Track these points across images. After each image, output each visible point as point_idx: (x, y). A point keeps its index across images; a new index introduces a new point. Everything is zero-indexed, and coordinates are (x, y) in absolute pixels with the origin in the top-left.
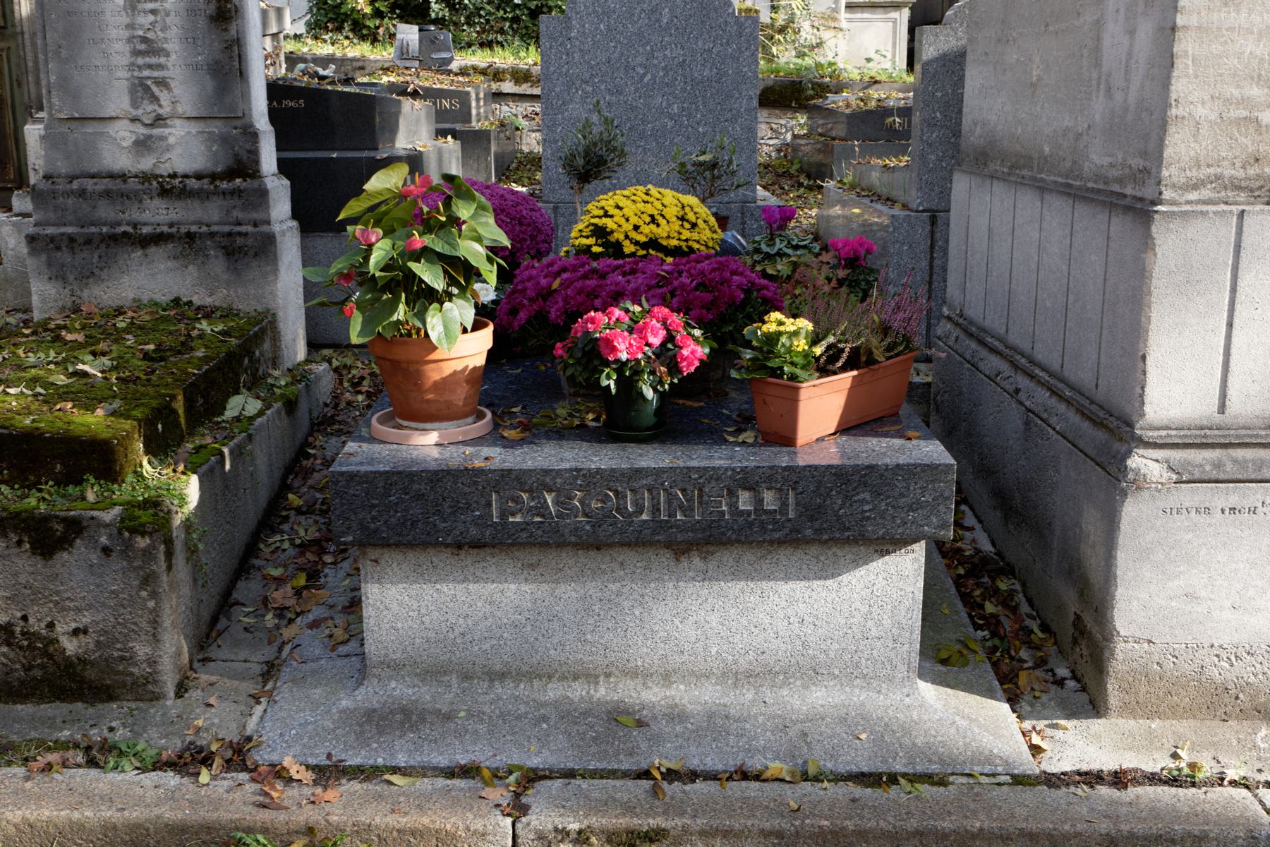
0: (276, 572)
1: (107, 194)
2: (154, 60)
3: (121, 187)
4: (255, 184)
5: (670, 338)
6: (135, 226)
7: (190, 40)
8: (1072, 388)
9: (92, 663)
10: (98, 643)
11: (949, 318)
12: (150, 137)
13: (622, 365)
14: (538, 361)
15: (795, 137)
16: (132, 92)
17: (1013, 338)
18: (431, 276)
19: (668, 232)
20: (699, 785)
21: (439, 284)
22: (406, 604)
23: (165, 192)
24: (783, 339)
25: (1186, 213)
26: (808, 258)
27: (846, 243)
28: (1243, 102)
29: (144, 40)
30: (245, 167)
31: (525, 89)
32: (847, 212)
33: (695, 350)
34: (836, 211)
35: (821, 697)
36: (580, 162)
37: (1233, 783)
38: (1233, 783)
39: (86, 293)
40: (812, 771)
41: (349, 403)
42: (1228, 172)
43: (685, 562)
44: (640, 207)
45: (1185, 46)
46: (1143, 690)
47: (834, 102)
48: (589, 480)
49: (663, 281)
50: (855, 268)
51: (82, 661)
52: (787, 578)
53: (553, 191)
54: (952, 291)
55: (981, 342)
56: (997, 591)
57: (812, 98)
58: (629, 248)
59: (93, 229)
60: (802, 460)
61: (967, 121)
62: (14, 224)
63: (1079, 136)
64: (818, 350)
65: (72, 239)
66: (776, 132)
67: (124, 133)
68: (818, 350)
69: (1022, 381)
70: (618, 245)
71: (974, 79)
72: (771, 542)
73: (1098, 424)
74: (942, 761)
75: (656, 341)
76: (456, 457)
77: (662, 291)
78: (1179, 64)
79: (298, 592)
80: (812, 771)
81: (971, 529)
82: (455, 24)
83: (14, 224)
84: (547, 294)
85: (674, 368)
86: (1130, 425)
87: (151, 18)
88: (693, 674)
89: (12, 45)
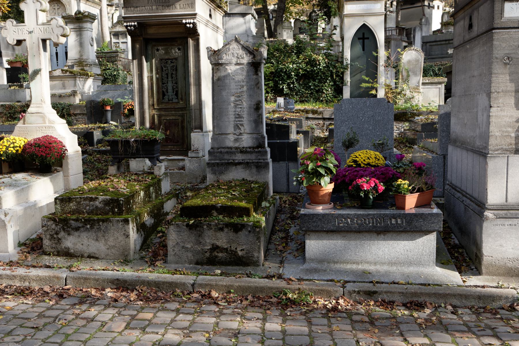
0: (277, 243)
1: (227, 152)
2: (240, 119)
3: (231, 151)
4: (264, 150)
5: (376, 185)
6: (234, 160)
7: (249, 114)
8: (474, 198)
9: (245, 257)
10: (246, 253)
11: (448, 184)
12: (238, 138)
13: (365, 191)
14: (346, 190)
15: (404, 130)
16: (234, 127)
17: (463, 188)
18: (322, 171)
19: (372, 161)
20: (384, 285)
21: (323, 173)
22: (314, 246)
23: (242, 152)
24: (402, 185)
25: (495, 156)
26: (408, 168)
27: (418, 164)
28: (506, 132)
29: (238, 114)
30: (261, 145)
31: (316, 116)
32: (421, 155)
33: (382, 187)
34: (416, 154)
35: (412, 269)
36: (347, 143)
37: (511, 288)
38: (511, 288)
39: (221, 177)
40: (410, 283)
41: (284, 207)
42: (504, 147)
43: (379, 235)
44: (365, 155)
45: (492, 120)
46: (491, 268)
47: (417, 120)
48: (358, 216)
49: (373, 173)
50: (420, 169)
51: (242, 257)
52: (403, 240)
53: (337, 150)
54: (449, 177)
55: (456, 190)
56: (459, 252)
57: (410, 117)
58: (362, 165)
59: (223, 161)
60: (407, 212)
61: (451, 131)
62: (189, 160)
63: (474, 138)
64: (410, 188)
65: (218, 164)
66: (399, 128)
67: (232, 137)
68: (410, 188)
69: (464, 198)
70: (360, 164)
71: (453, 120)
72: (400, 231)
73: (479, 206)
74: (441, 282)
75: (373, 186)
76: (327, 212)
77: (372, 175)
78: (491, 123)
79: (284, 247)
80: (410, 283)
81: (454, 239)
82: (292, 95)
83: (189, 160)
84: (345, 176)
85: (377, 191)
86: (485, 205)
87: (240, 109)
88: (381, 263)
89: (188, 112)
